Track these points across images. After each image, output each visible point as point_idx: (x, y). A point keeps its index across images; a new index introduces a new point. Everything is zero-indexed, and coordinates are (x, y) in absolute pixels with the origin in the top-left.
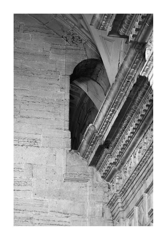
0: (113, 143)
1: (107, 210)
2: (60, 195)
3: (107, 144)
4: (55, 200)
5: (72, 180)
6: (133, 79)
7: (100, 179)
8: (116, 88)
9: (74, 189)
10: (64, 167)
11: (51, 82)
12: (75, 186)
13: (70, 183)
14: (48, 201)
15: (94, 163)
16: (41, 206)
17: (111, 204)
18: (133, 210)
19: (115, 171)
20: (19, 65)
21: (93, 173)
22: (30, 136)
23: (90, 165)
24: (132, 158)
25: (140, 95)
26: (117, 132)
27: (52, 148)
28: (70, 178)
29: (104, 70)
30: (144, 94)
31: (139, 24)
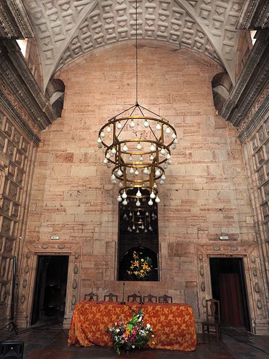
0: (241, 104)
1: (238, 140)
2: (214, 135)
3: (237, 107)
4: (212, 138)
5: (219, 128)
6: (257, 61)
7: (233, 126)
8: (220, 120)
9: (220, 132)
10: (214, 123)
11: (203, 85)
12: (220, 131)
13: (218, 130)
14: (208, 138)
15: (229, 119)
16: (206, 141)
17: (240, 137)
18: (255, 135)
19: (241, 120)
20: (62, 306)
21: (229, 124)
22: (196, 111)
23: (227, 120)
24: (253, 109)
25: (260, 70)
26: (244, 97)
27: (207, 115)
28: (217, 127)
29: (221, 96)
30: (263, 68)
31: (143, 267)
